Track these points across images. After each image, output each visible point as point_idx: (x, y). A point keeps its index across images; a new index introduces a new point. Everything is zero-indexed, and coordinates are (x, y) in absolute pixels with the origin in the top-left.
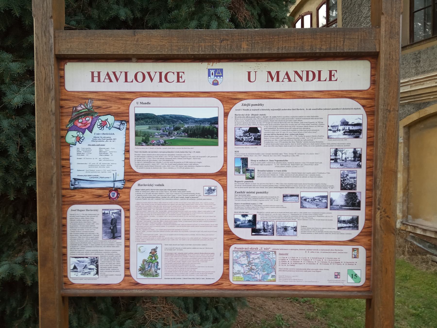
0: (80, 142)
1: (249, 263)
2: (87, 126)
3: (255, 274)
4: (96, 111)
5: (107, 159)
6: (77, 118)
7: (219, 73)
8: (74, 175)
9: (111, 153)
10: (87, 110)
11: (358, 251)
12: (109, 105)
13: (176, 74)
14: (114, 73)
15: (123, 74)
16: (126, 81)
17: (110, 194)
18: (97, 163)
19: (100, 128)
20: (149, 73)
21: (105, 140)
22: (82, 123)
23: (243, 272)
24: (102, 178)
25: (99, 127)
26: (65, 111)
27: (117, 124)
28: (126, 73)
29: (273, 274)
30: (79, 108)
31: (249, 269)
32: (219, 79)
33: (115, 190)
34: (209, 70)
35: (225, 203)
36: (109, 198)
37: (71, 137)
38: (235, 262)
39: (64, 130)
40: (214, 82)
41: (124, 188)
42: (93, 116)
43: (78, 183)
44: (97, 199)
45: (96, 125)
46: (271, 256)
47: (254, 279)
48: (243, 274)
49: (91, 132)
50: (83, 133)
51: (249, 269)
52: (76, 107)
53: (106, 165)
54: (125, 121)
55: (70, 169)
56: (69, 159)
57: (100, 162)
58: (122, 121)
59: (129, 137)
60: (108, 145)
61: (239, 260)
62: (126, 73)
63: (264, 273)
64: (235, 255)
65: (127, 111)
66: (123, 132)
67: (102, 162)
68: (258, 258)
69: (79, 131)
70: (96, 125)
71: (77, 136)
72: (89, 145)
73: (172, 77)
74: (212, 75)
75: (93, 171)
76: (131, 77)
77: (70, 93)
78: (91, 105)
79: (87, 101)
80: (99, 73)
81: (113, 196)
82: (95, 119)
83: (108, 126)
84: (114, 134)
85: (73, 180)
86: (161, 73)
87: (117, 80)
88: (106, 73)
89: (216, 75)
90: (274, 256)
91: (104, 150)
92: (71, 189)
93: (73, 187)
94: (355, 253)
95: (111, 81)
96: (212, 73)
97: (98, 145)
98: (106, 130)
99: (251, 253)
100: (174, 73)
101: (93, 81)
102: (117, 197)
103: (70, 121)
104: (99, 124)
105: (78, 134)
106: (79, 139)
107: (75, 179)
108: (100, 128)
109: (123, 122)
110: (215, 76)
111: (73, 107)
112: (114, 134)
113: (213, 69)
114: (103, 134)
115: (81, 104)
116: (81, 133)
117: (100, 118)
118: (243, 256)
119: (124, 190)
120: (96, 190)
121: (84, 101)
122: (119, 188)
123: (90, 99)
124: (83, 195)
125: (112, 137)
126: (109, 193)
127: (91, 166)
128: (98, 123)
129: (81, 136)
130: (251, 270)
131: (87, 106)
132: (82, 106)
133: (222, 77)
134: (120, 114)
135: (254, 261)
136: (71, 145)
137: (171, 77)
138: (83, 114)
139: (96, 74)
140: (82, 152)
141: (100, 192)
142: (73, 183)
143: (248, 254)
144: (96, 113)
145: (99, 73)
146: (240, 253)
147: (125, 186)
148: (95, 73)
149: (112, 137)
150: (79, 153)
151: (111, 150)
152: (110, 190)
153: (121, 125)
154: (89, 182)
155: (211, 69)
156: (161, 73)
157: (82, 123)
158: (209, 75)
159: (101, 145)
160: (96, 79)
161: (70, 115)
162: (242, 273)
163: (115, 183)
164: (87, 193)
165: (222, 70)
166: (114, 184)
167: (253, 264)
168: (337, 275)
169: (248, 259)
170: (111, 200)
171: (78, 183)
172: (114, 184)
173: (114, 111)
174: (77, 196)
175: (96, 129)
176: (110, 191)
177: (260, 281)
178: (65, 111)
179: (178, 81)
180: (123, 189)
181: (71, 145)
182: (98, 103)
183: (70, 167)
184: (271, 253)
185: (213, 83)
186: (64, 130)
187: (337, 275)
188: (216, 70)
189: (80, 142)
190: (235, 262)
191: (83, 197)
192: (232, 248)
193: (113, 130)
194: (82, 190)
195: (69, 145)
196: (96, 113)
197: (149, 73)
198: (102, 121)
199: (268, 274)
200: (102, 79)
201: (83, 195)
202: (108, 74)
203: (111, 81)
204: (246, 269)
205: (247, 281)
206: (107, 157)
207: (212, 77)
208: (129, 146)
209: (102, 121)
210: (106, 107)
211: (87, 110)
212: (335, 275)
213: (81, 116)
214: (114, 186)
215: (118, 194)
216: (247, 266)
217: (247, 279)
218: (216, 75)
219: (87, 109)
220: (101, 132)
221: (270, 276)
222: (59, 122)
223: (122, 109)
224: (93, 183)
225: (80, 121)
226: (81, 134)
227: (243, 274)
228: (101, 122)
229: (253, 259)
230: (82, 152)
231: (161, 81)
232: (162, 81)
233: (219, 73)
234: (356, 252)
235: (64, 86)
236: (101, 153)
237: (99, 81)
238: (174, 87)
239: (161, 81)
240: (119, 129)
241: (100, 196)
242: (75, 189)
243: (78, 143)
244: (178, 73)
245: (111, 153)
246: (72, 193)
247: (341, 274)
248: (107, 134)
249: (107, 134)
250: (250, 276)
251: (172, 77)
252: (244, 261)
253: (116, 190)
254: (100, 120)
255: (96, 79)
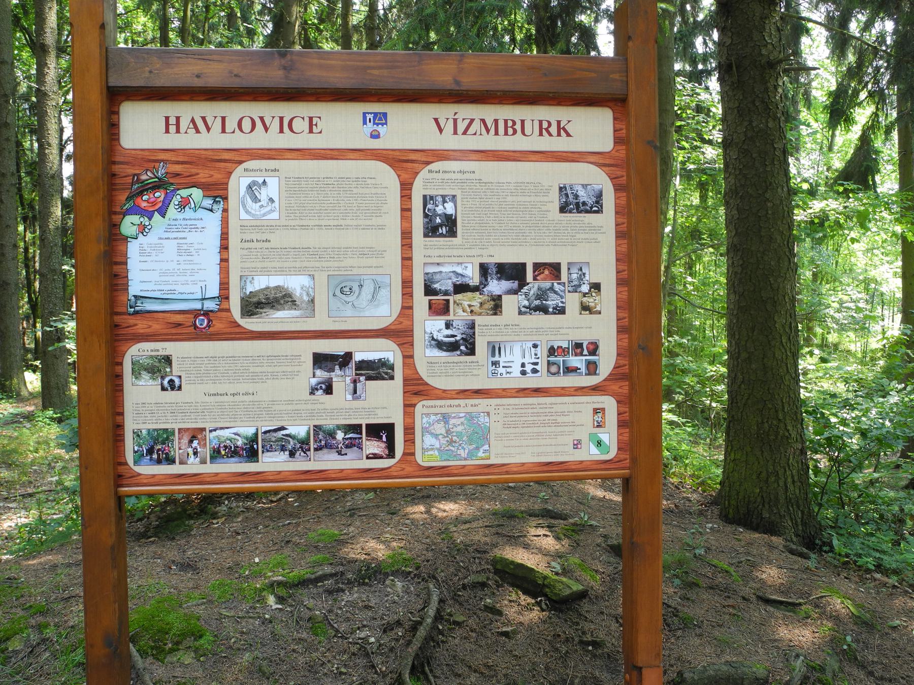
0: (145, 234)
1: (448, 432)
2: (157, 207)
3: (458, 449)
4: (172, 181)
5: (191, 262)
6: (141, 193)
7: (380, 119)
8: (135, 289)
9: (197, 250)
10: (156, 180)
11: (604, 414)
12: (194, 171)
13: (307, 120)
14: (204, 119)
15: (219, 120)
16: (224, 131)
17: (195, 321)
18: (174, 269)
19: (180, 210)
20: (262, 119)
21: (187, 230)
22: (147, 201)
23: (438, 447)
24: (182, 293)
25: (177, 207)
26: (118, 181)
27: (208, 202)
28: (223, 119)
29: (486, 447)
30: (144, 177)
31: (448, 441)
32: (380, 128)
33: (204, 315)
34: (364, 114)
35: (224, 248)
36: (195, 329)
37: (129, 224)
38: (425, 430)
39: (119, 213)
40: (373, 133)
41: (220, 310)
42: (166, 189)
43: (142, 303)
44: (174, 331)
45: (172, 204)
46: (483, 419)
47: (457, 457)
48: (439, 450)
49: (163, 215)
50: (150, 219)
51: (448, 441)
52: (138, 175)
53: (189, 271)
54: (221, 197)
55: (128, 280)
56: (126, 263)
57: (178, 267)
58: (216, 197)
59: (228, 224)
60: (192, 237)
61: (432, 427)
62: (223, 119)
63: (471, 447)
64: (425, 420)
65: (225, 181)
66: (218, 214)
67: (182, 267)
68: (462, 424)
69: (142, 216)
70: (172, 204)
71: (139, 223)
72: (161, 239)
73: (301, 125)
74: (370, 121)
75: (166, 283)
76: (231, 125)
77: (128, 151)
78: (163, 171)
79: (157, 165)
80: (178, 119)
81: (201, 325)
82: (170, 195)
83: (193, 206)
84: (201, 219)
85: (133, 298)
86: (281, 119)
87: (208, 129)
88: (190, 120)
89: (376, 122)
90: (487, 420)
91: (185, 247)
92: (129, 314)
93: (133, 310)
94: (598, 417)
95: (198, 131)
96: (370, 119)
97: (175, 238)
98: (188, 214)
99: (450, 417)
100: (303, 118)
101: (167, 131)
102: (209, 326)
103: (129, 198)
104: (177, 203)
105: (142, 219)
106: (143, 229)
107: (135, 296)
108: (180, 210)
109: (217, 199)
110: (374, 123)
111: (134, 175)
112: (201, 219)
113: (371, 113)
114: (184, 219)
115: (147, 170)
116: (146, 219)
117: (178, 192)
118: (438, 421)
119: (220, 314)
120: (172, 315)
121: (152, 165)
122: (211, 311)
123: (163, 161)
124: (150, 323)
125: (199, 224)
126: (193, 320)
127: (164, 273)
128: (176, 200)
129: (147, 223)
130: (451, 442)
131: (158, 173)
132: (149, 173)
133: (385, 126)
134: (213, 185)
135: (455, 429)
136: (129, 239)
137: (298, 125)
138: (150, 186)
139: (172, 121)
140: (148, 250)
141: (179, 318)
142: (132, 303)
143: (445, 418)
144: (172, 184)
145: (178, 119)
146: (433, 417)
147: (222, 307)
148: (170, 119)
149: (199, 224)
150: (142, 252)
151: (196, 246)
152: (196, 313)
153: (214, 205)
154: (160, 301)
155: (368, 113)
156: (281, 119)
157: (147, 201)
158: (365, 123)
159: (180, 238)
160: (172, 129)
161: (128, 189)
162: (437, 449)
163: (205, 302)
164: (157, 321)
165: (385, 115)
166: (203, 305)
167: (455, 434)
168: (577, 444)
169: (447, 426)
170: (198, 331)
171: (142, 303)
172: (203, 305)
173: (203, 180)
174: (140, 326)
175: (172, 211)
176: (196, 317)
177: (465, 459)
178: (118, 181)
179: (311, 131)
180: (219, 313)
181: (129, 239)
182: (177, 168)
183: (127, 277)
184: (482, 414)
185: (371, 134)
186: (119, 213)
187: (577, 445)
188: (375, 114)
189: (145, 234)
190: (425, 430)
191: (150, 327)
192: (419, 409)
193: (202, 213)
194: (147, 315)
195: (125, 239)
196: (172, 184)
197: (262, 119)
198: (181, 197)
199: (477, 448)
200: (183, 128)
201: (150, 323)
202: (193, 121)
203: (198, 131)
204: (444, 441)
205: (445, 460)
206: (190, 258)
207: (370, 125)
208: (227, 239)
209: (181, 197)
210: (188, 174)
211: (156, 180)
212: (574, 445)
213: (147, 190)
214: (203, 308)
215: (209, 321)
216: (445, 437)
217: (445, 457)
218: (376, 122)
219: (157, 177)
220: (180, 216)
221: (481, 451)
222: (110, 200)
223: (217, 176)
224: (168, 303)
225: (145, 197)
226: (146, 221)
227: (439, 450)
228: (180, 200)
229: (455, 425)
230: (148, 250)
231: (281, 131)
232: (284, 131)
233: (380, 119)
234: (600, 415)
235: (118, 140)
236: (180, 251)
237: (178, 131)
238: (303, 141)
239: (281, 131)
240: (211, 210)
241: (179, 325)
242: (136, 313)
243: (141, 235)
244: (311, 119)
245: (197, 250)
246: (131, 321)
247: (583, 442)
248: (190, 219)
249: (190, 219)
250: (450, 452)
251: (301, 125)
252: (440, 429)
253: (207, 313)
254: (178, 197)
255: (172, 129)
